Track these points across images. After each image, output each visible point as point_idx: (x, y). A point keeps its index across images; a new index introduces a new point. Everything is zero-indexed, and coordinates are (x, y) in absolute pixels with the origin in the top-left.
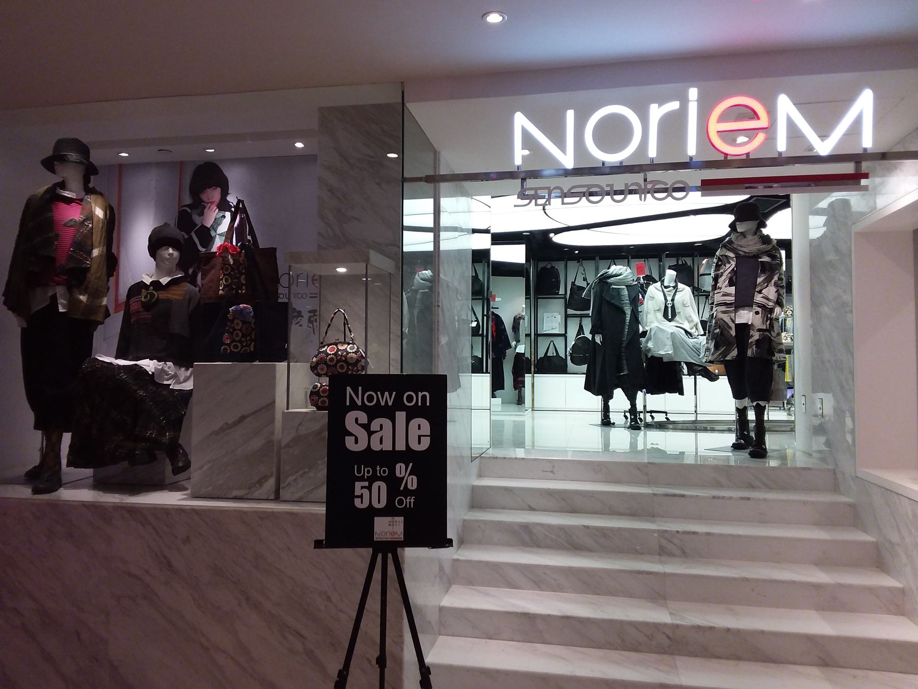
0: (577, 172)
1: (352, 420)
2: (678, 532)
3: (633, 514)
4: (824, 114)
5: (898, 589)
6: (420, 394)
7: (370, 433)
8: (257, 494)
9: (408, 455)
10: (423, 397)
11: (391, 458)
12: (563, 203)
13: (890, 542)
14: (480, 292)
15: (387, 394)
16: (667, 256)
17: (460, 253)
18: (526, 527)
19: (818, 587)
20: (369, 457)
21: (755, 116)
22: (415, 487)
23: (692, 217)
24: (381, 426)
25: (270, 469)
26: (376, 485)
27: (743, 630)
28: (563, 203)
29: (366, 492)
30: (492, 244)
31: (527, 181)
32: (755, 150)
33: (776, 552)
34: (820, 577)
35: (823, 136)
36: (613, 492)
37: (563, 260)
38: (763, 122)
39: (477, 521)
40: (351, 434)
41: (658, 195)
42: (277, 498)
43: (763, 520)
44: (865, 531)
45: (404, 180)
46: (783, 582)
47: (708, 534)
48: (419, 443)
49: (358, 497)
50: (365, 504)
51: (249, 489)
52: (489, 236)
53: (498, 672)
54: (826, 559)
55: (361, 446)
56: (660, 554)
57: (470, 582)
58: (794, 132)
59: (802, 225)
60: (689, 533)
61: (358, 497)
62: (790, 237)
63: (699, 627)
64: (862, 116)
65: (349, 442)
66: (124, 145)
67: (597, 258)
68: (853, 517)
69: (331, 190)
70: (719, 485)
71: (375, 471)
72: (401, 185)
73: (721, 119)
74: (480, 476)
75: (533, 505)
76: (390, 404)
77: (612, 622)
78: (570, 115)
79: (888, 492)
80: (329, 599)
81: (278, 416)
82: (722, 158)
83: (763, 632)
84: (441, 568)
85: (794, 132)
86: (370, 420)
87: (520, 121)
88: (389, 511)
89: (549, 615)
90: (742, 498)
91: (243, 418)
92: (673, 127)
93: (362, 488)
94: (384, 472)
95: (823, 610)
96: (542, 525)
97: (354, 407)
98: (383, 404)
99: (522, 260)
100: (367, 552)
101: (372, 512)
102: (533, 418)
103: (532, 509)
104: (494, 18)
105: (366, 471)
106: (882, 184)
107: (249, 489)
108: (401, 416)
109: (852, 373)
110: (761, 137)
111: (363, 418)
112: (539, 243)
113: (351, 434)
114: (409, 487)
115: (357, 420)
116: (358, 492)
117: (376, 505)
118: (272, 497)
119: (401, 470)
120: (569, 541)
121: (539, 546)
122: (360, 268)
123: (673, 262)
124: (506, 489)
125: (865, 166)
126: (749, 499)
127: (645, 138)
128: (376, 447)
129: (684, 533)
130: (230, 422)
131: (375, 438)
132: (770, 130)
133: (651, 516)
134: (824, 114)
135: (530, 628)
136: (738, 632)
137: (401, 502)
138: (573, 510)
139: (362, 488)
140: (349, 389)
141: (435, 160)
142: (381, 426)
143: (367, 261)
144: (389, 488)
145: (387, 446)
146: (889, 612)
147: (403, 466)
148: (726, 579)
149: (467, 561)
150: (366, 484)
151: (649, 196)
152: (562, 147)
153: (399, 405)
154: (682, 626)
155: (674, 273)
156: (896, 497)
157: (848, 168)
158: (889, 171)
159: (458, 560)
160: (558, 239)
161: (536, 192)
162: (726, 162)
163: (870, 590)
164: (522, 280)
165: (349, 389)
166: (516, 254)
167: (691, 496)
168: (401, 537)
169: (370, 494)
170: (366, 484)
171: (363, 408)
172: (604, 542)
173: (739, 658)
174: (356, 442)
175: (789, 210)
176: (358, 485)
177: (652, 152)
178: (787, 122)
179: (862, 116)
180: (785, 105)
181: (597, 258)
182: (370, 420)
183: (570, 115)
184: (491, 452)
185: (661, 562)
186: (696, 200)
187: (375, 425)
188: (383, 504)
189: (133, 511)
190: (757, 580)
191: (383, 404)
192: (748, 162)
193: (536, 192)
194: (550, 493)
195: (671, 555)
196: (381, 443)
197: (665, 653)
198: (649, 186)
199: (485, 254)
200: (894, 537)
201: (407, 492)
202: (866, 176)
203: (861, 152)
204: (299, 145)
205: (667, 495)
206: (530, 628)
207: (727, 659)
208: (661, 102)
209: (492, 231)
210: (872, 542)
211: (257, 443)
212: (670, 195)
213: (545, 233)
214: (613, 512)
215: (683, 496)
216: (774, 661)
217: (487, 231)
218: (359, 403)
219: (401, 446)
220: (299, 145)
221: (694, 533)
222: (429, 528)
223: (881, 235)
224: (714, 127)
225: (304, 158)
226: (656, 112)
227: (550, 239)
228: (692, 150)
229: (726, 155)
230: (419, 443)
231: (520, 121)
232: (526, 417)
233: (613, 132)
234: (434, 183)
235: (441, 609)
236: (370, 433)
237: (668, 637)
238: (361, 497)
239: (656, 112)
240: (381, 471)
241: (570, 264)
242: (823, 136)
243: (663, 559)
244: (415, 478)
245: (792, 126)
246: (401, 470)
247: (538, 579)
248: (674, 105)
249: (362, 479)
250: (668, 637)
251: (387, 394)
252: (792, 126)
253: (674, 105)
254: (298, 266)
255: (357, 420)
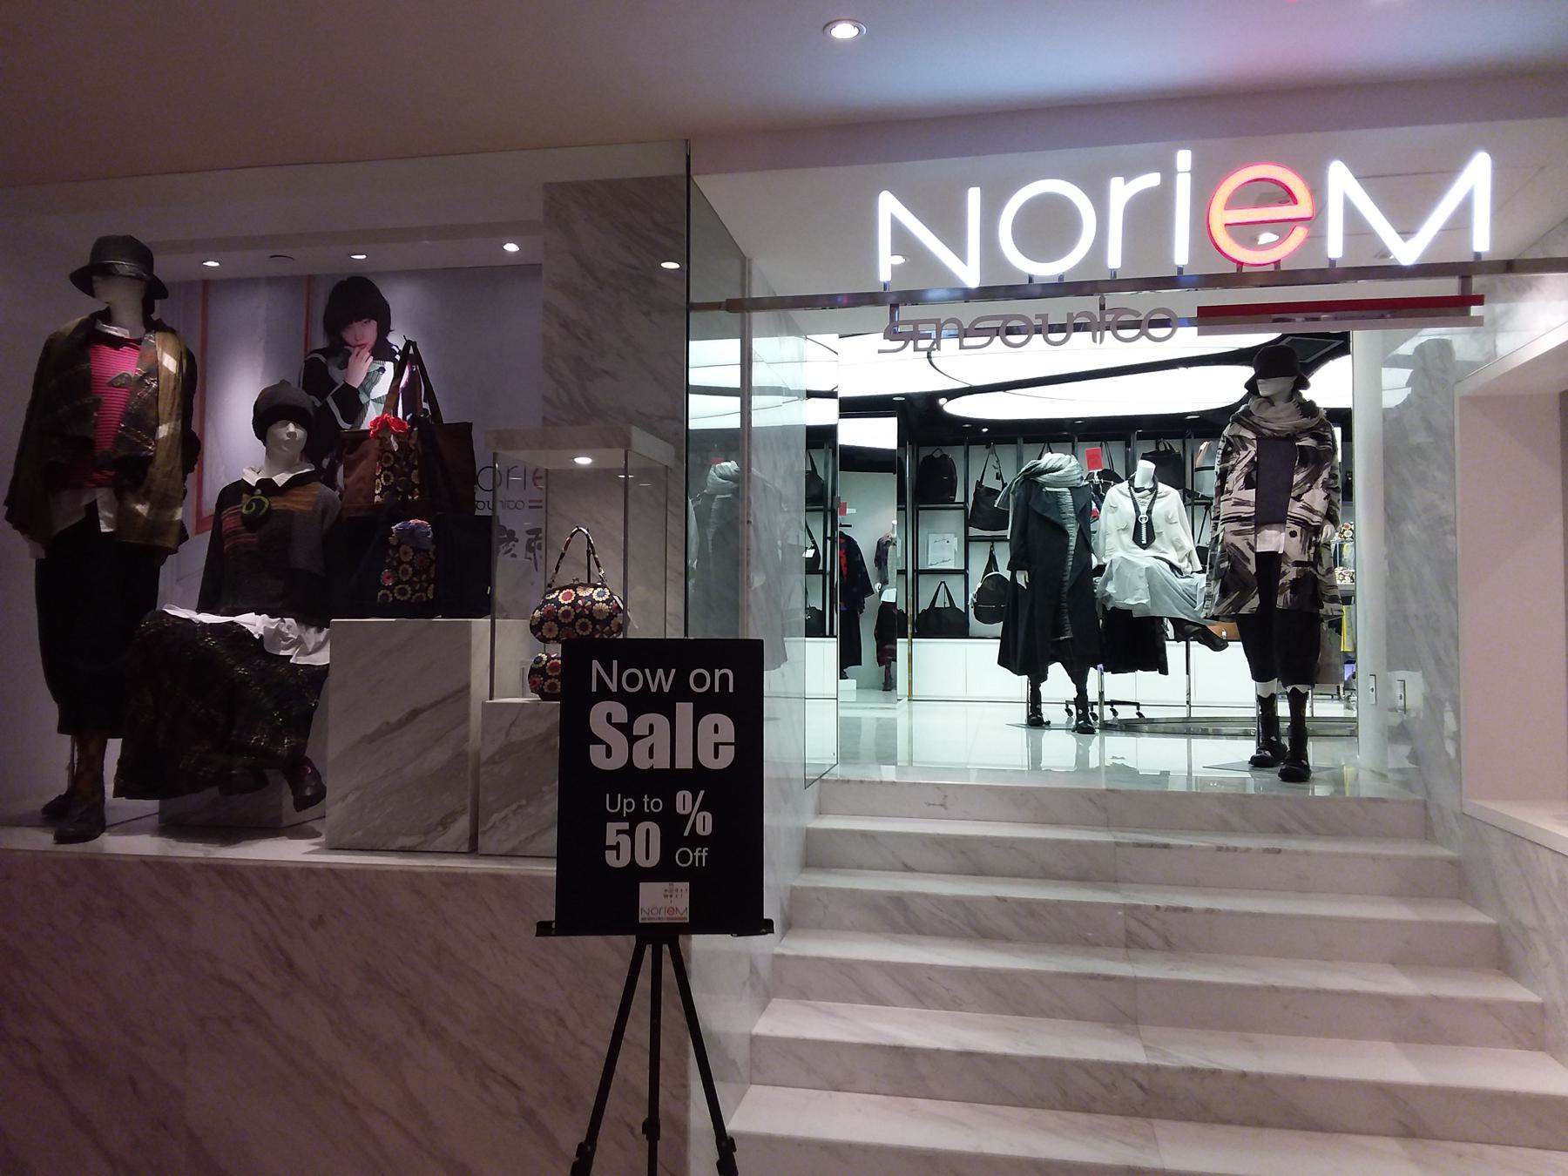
0: (986, 293)
1: (601, 716)
2: (1158, 908)
3: (1081, 878)
4: (1407, 194)
5: (1534, 1005)
6: (718, 673)
7: (632, 740)
8: (438, 844)
9: (697, 777)
10: (722, 677)
11: (668, 781)
12: (962, 347)
13: (1520, 925)
14: (820, 499)
15: (660, 672)
16: (1140, 437)
17: (785, 431)
18: (898, 900)
19: (1397, 1002)
20: (631, 780)
21: (1290, 197)
22: (709, 831)
23: (1182, 370)
24: (651, 726)
25: (461, 801)
26: (641, 828)
27: (1269, 1076)
28: (962, 347)
29: (625, 840)
30: (841, 417)
31: (901, 309)
32: (1289, 256)
33: (1325, 942)
34: (1401, 984)
35: (1406, 233)
36: (1046, 840)
37: (961, 444)
38: (1304, 208)
39: (815, 889)
40: (599, 741)
41: (1123, 333)
42: (473, 850)
43: (1303, 888)
44: (1477, 906)
45: (690, 307)
46: (1338, 994)
47: (1210, 911)
48: (716, 756)
49: (611, 848)
50: (624, 861)
51: (426, 834)
52: (835, 403)
53: (851, 1147)
54: (1410, 953)
55: (617, 762)
56: (1127, 946)
57: (802, 993)
58: (1356, 226)
59: (1370, 384)
60: (1177, 909)
61: (611, 848)
62: (1349, 405)
63: (1194, 1070)
64: (1473, 199)
65: (597, 755)
66: (212, 248)
67: (1020, 441)
68: (1458, 882)
69: (565, 324)
70: (1227, 828)
71: (640, 804)
72: (685, 315)
73: (1231, 204)
74: (820, 812)
75: (910, 863)
76: (666, 689)
77: (1045, 1061)
78: (974, 196)
79: (1517, 839)
80: (561, 1022)
81: (476, 710)
82: (1233, 269)
83: (1303, 1079)
84: (754, 970)
85: (1356, 226)
86: (632, 717)
87: (889, 206)
88: (665, 872)
89: (938, 1050)
90: (1268, 851)
92: (1149, 216)
93: (619, 832)
94: (657, 805)
95: (1406, 1040)
96: (926, 896)
97: (604, 694)
98: (654, 689)
99: (892, 444)
100: (627, 942)
101: (635, 874)
102: (910, 713)
103: (908, 869)
104: (844, 31)
105: (625, 805)
106: (1506, 313)
107: (426, 834)
108: (684, 710)
109: (1455, 637)
110: (1300, 234)
111: (620, 713)
112: (920, 416)
113: (599, 741)
114: (699, 831)
115: (609, 716)
116: (611, 839)
117: (642, 861)
118: (465, 848)
119: (684, 801)
120: (972, 924)
121: (920, 932)
122: (615, 458)
123: (1149, 447)
124: (865, 835)
125: (1478, 284)
126: (1279, 851)
127: (1101, 235)
128: (642, 762)
129: (1169, 909)
130: (393, 720)
131: (641, 748)
132: (1315, 222)
133: (1111, 880)
134: (1407, 194)
135: (906, 1072)
136: (1261, 1079)
137: (684, 858)
138: (980, 871)
139: (619, 832)
140: (596, 664)
141: (743, 274)
142: (651, 726)
143: (627, 445)
144: (664, 833)
145: (662, 762)
146: (1519, 1044)
147: (689, 795)
148: (1241, 988)
149: (798, 958)
150: (626, 826)
151: (1108, 334)
152: (960, 250)
153: (681, 691)
154: (1165, 1068)
155: (1152, 466)
156: (1530, 848)
157: (1448, 287)
158: (1519, 291)
159: (782, 956)
160: (953, 408)
161: (916, 328)
162: (1240, 277)
163: (1487, 1006)
164: (892, 479)
165: (596, 664)
166: (881, 434)
167: (1181, 847)
168: (684, 916)
169: (633, 844)
170: (626, 826)
171: (620, 696)
172: (1031, 924)
173: (1262, 1124)
174: (609, 754)
175: (1348, 358)
176: (612, 827)
177: (1114, 260)
178: (1345, 208)
179: (1473, 199)
180: (1341, 180)
181: (1020, 441)
182: (632, 717)
183: (974, 196)
184: (839, 772)
185: (1128, 960)
186: (1189, 341)
187: (640, 726)
188: (654, 860)
190: (1293, 990)
191: (654, 689)
192: (1278, 276)
193: (916, 328)
194: (939, 841)
195: (1146, 947)
196: (651, 756)
197: (1136, 1114)
198: (1109, 318)
199: (829, 433)
200: (1528, 917)
201: (695, 840)
202: (1479, 300)
203: (1470, 259)
204: (511, 248)
205: (1139, 845)
206: (906, 1072)
207: (1242, 1124)
208: (1129, 174)
209: (840, 395)
210: (1490, 926)
211: (438, 756)
212: (1144, 333)
213: (932, 398)
214: (1048, 875)
215: (1166, 846)
216: (1322, 1129)
217: (831, 395)
218: (614, 688)
219: (684, 762)
220: (511, 248)
221: (1186, 910)
222: (733, 902)
223: (1505, 400)
224: (1220, 216)
225: (520, 270)
226: (1121, 192)
227: (940, 408)
228: (1181, 255)
229: (1240, 264)
230: (716, 756)
231: (889, 206)
232: (898, 712)
233: (1047, 226)
234: (741, 312)
235: (754, 1039)
236: (632, 740)
237: (1141, 1087)
238: (617, 847)
239: (1121, 192)
240: (651, 804)
241: (974, 450)
242: (1406, 233)
243: (1132, 953)
244: (709, 816)
245: (1352, 215)
246: (684, 801)
247: (918, 988)
248: (1152, 180)
249: (618, 817)
250: (1141, 1087)
251: (660, 672)
252: (1352, 215)
253: (1152, 180)
254: (509, 453)
255: (609, 716)
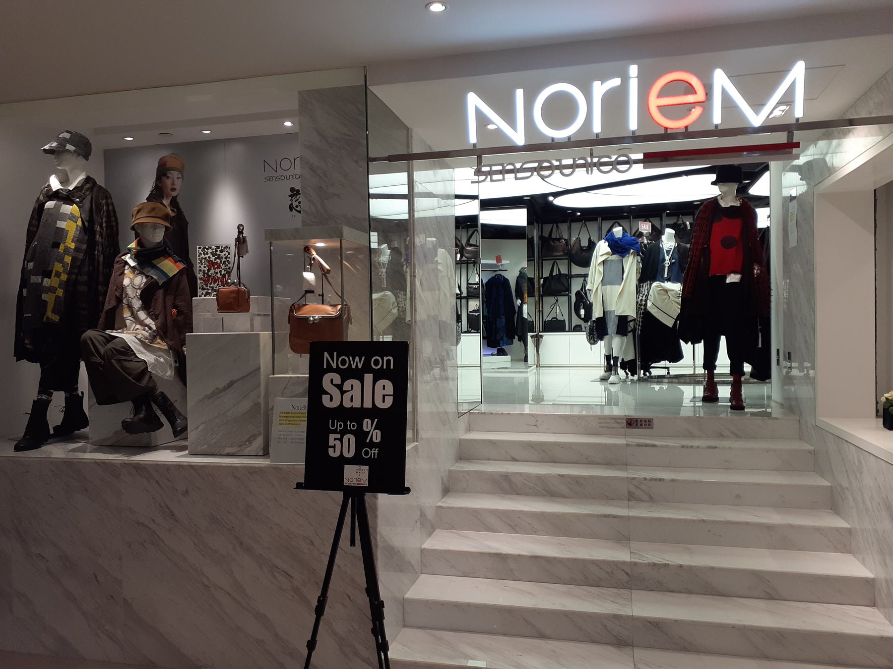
0: (527, 148)
1: (329, 381)
2: (645, 479)
3: (608, 464)
4: (756, 89)
5: (847, 529)
6: (385, 359)
7: (343, 392)
8: (247, 451)
9: (374, 412)
10: (386, 361)
11: (359, 414)
12: (516, 178)
13: (841, 486)
14: (467, 260)
15: (357, 358)
16: (668, 215)
17: (439, 221)
18: (506, 477)
19: (769, 528)
20: (342, 413)
21: (691, 90)
22: (379, 440)
23: (684, 177)
24: (352, 386)
25: (258, 427)
26: (346, 437)
27: (695, 567)
28: (516, 178)
29: (338, 443)
30: (482, 210)
31: (487, 154)
32: (694, 122)
33: (738, 496)
34: (775, 518)
35: (757, 106)
36: (596, 444)
37: (566, 222)
38: (700, 96)
39: (463, 471)
40: (327, 393)
41: (604, 168)
42: (266, 453)
43: (727, 466)
44: (822, 476)
45: (370, 160)
46: (738, 523)
47: (673, 480)
48: (384, 402)
49: (331, 447)
50: (337, 454)
51: (240, 446)
52: (476, 203)
53: (469, 605)
54: (783, 500)
55: (335, 404)
56: (629, 500)
57: (452, 527)
58: (728, 104)
59: (777, 184)
60: (655, 480)
61: (331, 447)
62: (768, 194)
63: (655, 564)
64: (794, 90)
65: (325, 400)
66: (129, 131)
67: (600, 219)
68: (816, 462)
69: (312, 169)
70: (691, 436)
71: (346, 425)
72: (370, 162)
73: (660, 95)
74: (469, 430)
75: (515, 457)
76: (360, 367)
77: (575, 560)
78: (520, 94)
79: (841, 440)
80: (312, 543)
81: (262, 377)
82: (662, 132)
83: (713, 568)
84: (422, 514)
85: (728, 104)
86: (343, 381)
87: (473, 101)
88: (357, 460)
89: (519, 555)
90: (709, 447)
91: (231, 384)
92: (615, 103)
93: (335, 439)
94: (354, 426)
95: (774, 548)
96: (521, 474)
97: (330, 369)
98: (354, 367)
99: (524, 223)
100: (339, 496)
101: (342, 461)
102: (539, 374)
103: (515, 460)
105: (339, 425)
106: (839, 145)
107: (240, 446)
108: (368, 378)
109: (813, 329)
110: (696, 112)
111: (337, 379)
112: (539, 208)
113: (327, 393)
114: (374, 440)
115: (332, 380)
116: (331, 443)
117: (346, 455)
118: (261, 453)
119: (367, 425)
120: (544, 489)
121: (518, 494)
122: (335, 244)
123: (672, 221)
124: (492, 442)
125: (798, 136)
126: (716, 447)
127: (589, 115)
128: (347, 404)
129: (651, 479)
130: (220, 387)
131: (347, 396)
132: (706, 104)
133: (625, 465)
134: (756, 89)
135: (503, 567)
136: (690, 568)
137: (366, 453)
138: (554, 461)
139: (335, 439)
140: (326, 354)
141: (408, 137)
142: (352, 386)
143: (341, 237)
144: (358, 439)
145: (357, 404)
146: (837, 550)
147: (369, 421)
148: (685, 521)
149: (449, 508)
150: (338, 436)
151: (595, 168)
152: (512, 122)
153: (367, 368)
154: (640, 563)
155: (673, 232)
156: (845, 443)
157: (780, 138)
158: (844, 135)
159: (441, 507)
160: (560, 202)
161: (503, 167)
162: (667, 135)
163: (819, 530)
164: (524, 243)
165: (326, 354)
166: (518, 217)
167: (662, 446)
168: (366, 484)
169: (342, 446)
170: (338, 436)
171: (337, 370)
172: (577, 489)
173: (690, 592)
174: (331, 399)
175: (768, 172)
176: (332, 437)
177: (597, 128)
178: (723, 96)
179: (794, 90)
180: (720, 79)
181: (600, 219)
182: (343, 381)
183: (520, 94)
184: (483, 408)
185: (629, 507)
186: (638, 171)
187: (347, 386)
188: (352, 454)
189: (139, 468)
190: (713, 522)
191: (354, 367)
192: (687, 134)
193: (503, 167)
194: (531, 445)
195: (639, 500)
196: (352, 401)
197: (623, 587)
198: (595, 160)
199: (474, 219)
201: (372, 445)
202: (797, 145)
203: (794, 122)
204: (288, 124)
205: (639, 445)
206: (503, 567)
207: (680, 592)
208: (603, 80)
209: (481, 197)
210: (827, 486)
211: (246, 405)
212: (614, 168)
213: (545, 196)
214: (590, 462)
215: (654, 446)
216: (724, 596)
217: (474, 197)
218: (334, 366)
219: (368, 404)
220: (288, 124)
221: (660, 480)
222: (391, 476)
223: (843, 195)
224: (654, 102)
225: (289, 137)
226: (599, 89)
227: (551, 203)
228: (633, 125)
229: (666, 129)
230: (384, 402)
231: (473, 101)
232: (531, 375)
233: (561, 109)
234: (404, 159)
235: (423, 551)
236: (343, 392)
237: (627, 574)
238: (334, 447)
239: (599, 89)
240: (352, 425)
241: (574, 225)
242: (757, 106)
243: (631, 503)
244: (379, 432)
245: (726, 99)
246: (367, 425)
247: (513, 523)
248: (616, 82)
249: (335, 432)
250: (627, 574)
251: (357, 358)
252: (726, 99)
253: (616, 82)
254: (279, 242)
255: (332, 380)
